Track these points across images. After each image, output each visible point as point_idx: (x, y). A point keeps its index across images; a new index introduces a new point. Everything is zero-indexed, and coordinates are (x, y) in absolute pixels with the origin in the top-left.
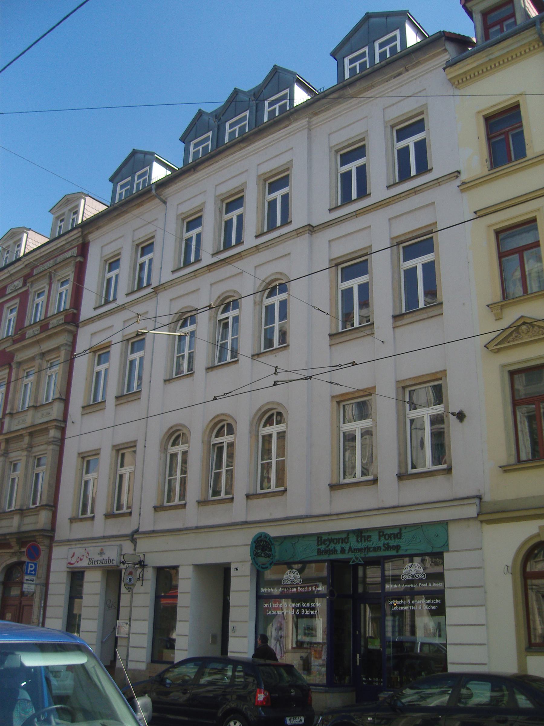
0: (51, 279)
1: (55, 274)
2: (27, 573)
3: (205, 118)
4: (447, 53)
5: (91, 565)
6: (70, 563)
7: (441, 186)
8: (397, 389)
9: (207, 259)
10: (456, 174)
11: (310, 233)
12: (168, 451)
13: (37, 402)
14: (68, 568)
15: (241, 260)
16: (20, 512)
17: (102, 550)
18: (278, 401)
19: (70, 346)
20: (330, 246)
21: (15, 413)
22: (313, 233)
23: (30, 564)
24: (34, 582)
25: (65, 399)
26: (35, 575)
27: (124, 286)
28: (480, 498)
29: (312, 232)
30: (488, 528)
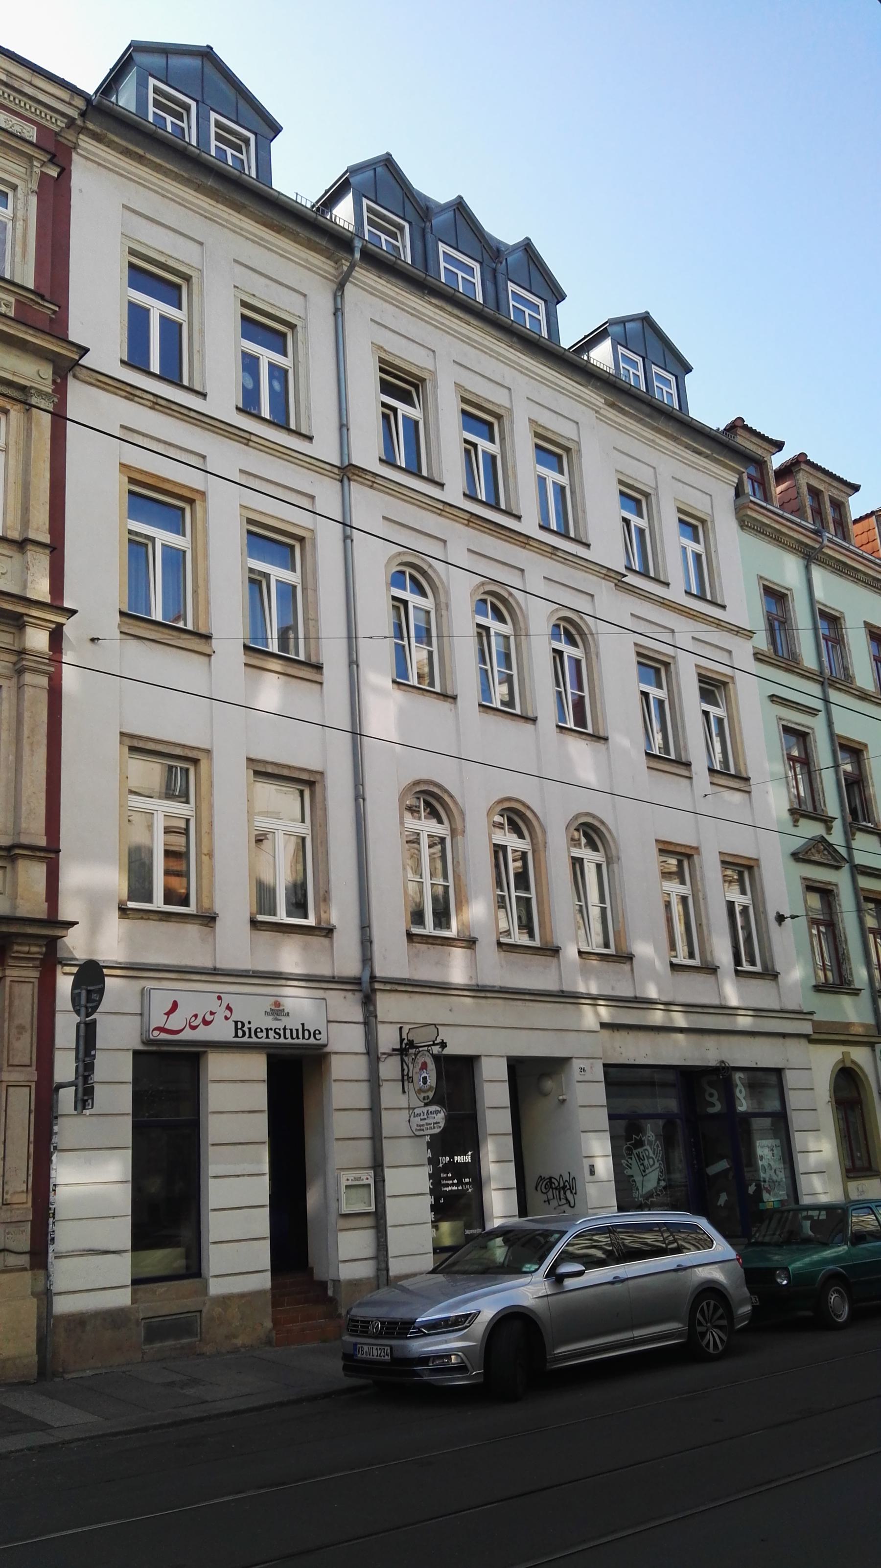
5: (246, 1039)
7: (737, 637)
15: (521, 547)
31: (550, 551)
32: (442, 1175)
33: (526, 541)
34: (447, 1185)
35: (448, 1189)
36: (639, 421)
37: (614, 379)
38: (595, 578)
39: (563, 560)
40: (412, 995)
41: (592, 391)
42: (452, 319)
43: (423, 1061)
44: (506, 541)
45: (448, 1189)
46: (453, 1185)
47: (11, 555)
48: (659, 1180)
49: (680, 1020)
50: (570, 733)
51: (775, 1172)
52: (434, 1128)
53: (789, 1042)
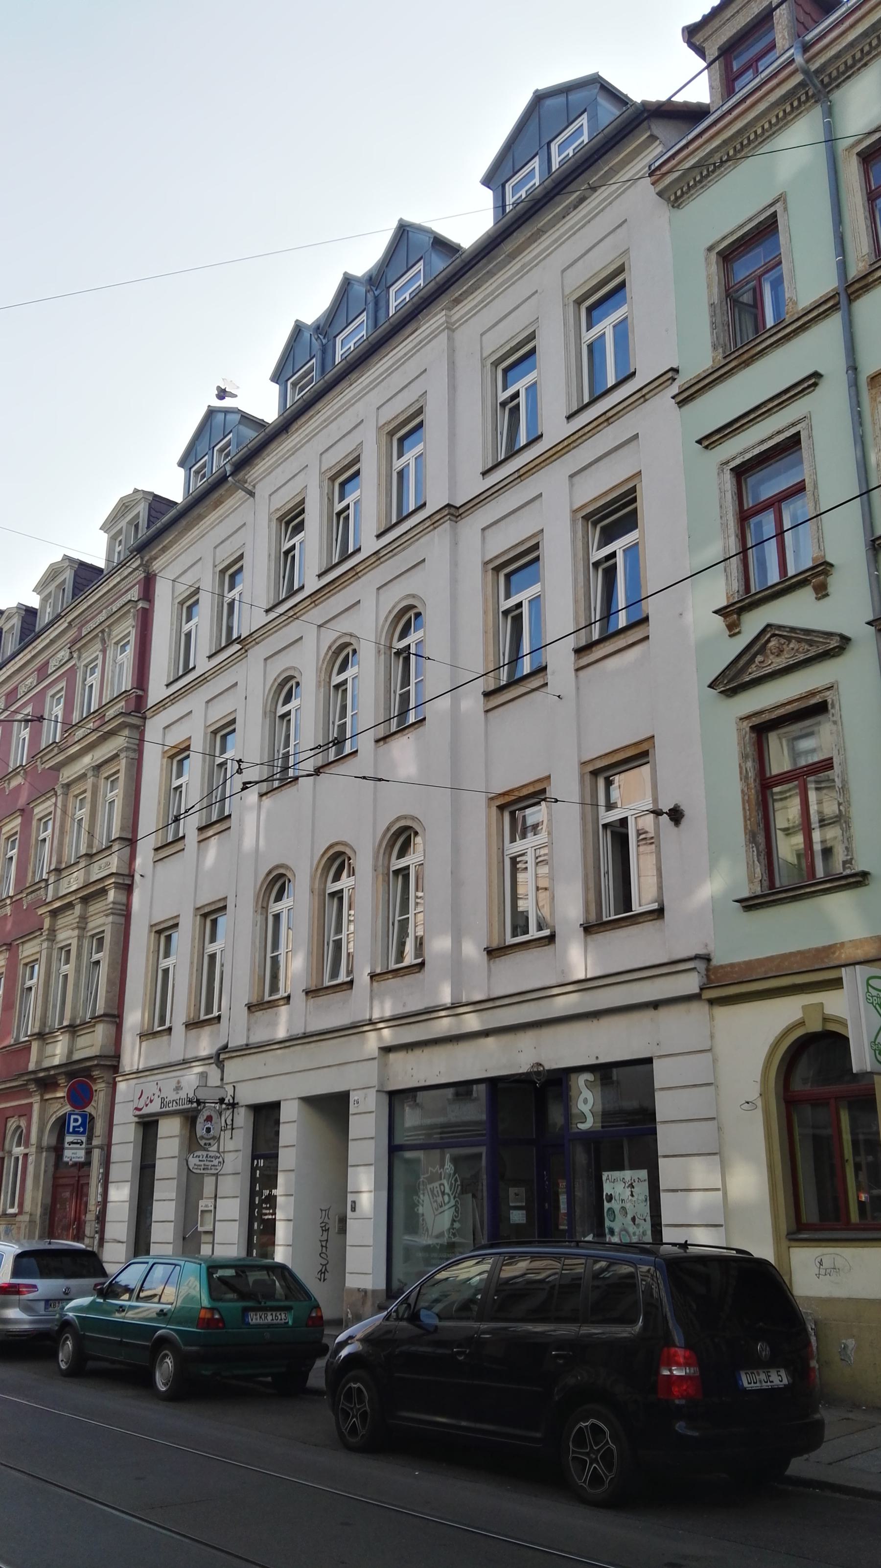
0: (103, 641)
1: (109, 635)
2: (69, 1132)
3: (307, 335)
4: (658, 142)
6: (137, 1109)
8: (582, 776)
9: (312, 584)
10: (670, 375)
11: (454, 519)
12: (270, 911)
13: (92, 848)
14: (135, 1116)
15: (357, 579)
16: (70, 1029)
17: (179, 1082)
18: (412, 814)
19: (134, 750)
20: (484, 539)
21: (64, 869)
22: (459, 518)
23: (73, 1117)
24: (83, 1146)
25: (130, 841)
26: (83, 1133)
27: (203, 645)
28: (707, 959)
29: (457, 517)
30: (721, 1012)
31: (374, 559)
32: (264, 1206)
33: (354, 573)
34: (266, 1214)
35: (266, 1217)
36: (491, 274)
37: (416, 298)
38: (427, 537)
39: (391, 554)
40: (244, 1058)
41: (427, 322)
42: (310, 423)
43: (209, 1114)
44: (344, 588)
45: (266, 1217)
46: (269, 1214)
47: (542, 683)
48: (453, 1221)
49: (472, 1022)
50: (393, 738)
51: (633, 1219)
52: (211, 1169)
53: (664, 1013)
